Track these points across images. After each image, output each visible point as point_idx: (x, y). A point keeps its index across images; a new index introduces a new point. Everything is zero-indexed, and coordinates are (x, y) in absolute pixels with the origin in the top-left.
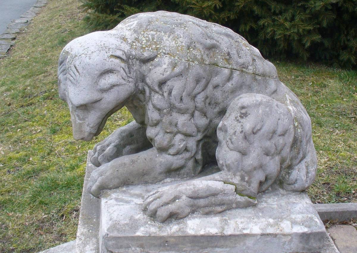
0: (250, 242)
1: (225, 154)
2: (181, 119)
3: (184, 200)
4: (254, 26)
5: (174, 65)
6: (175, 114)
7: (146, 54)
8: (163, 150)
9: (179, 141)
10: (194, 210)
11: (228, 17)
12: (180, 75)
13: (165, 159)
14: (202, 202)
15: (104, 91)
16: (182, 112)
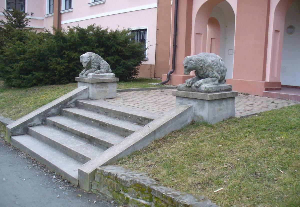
0: (107, 76)
1: (102, 67)
2: (96, 64)
3: (99, 72)
4: (75, 73)
5: (94, 57)
6: (95, 63)
7: (91, 56)
8: (94, 68)
9: (96, 67)
10: (100, 73)
11: (67, 71)
12: (95, 58)
13: (94, 69)
14: (101, 72)
15: (88, 60)
16: (96, 63)
